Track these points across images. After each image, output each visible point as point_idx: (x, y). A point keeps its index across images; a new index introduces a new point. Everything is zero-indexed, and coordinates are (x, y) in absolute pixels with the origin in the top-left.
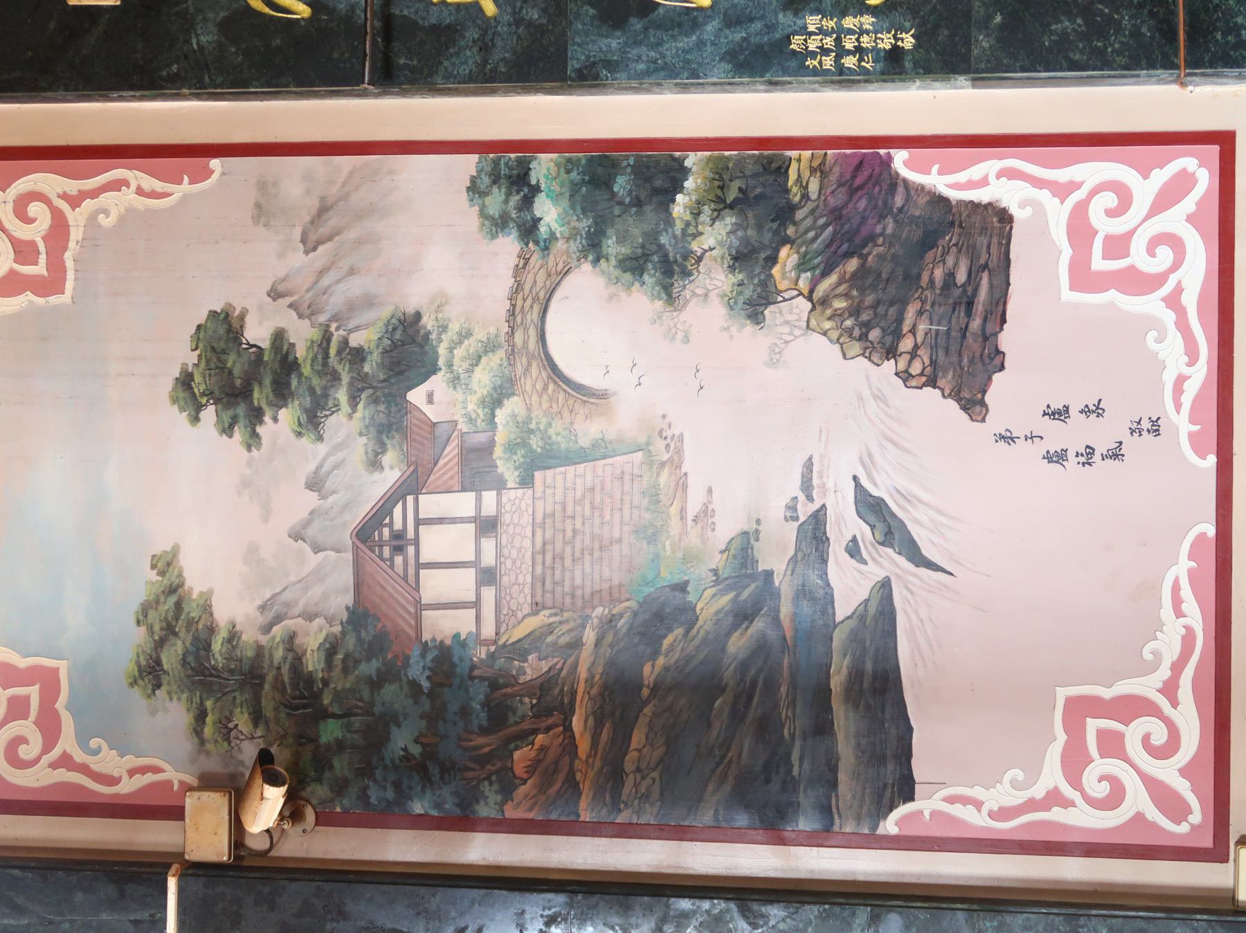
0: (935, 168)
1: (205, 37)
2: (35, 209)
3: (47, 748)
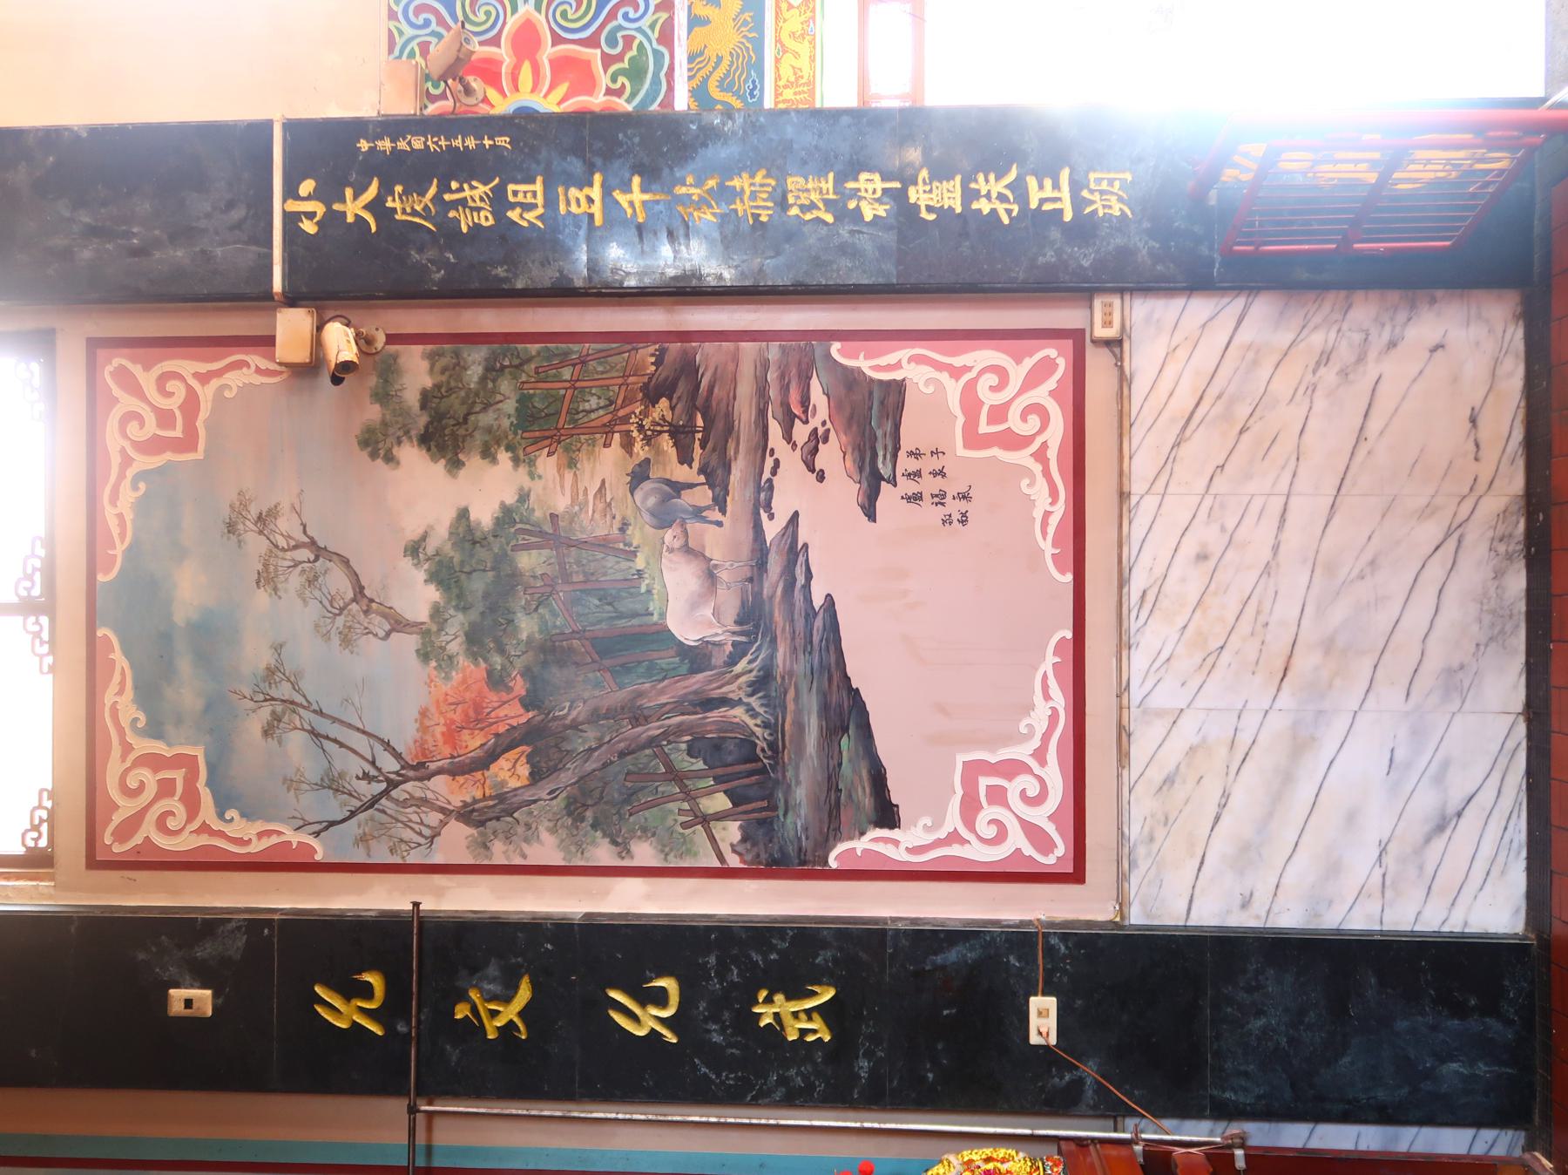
2: (172, 385)
3: (190, 819)
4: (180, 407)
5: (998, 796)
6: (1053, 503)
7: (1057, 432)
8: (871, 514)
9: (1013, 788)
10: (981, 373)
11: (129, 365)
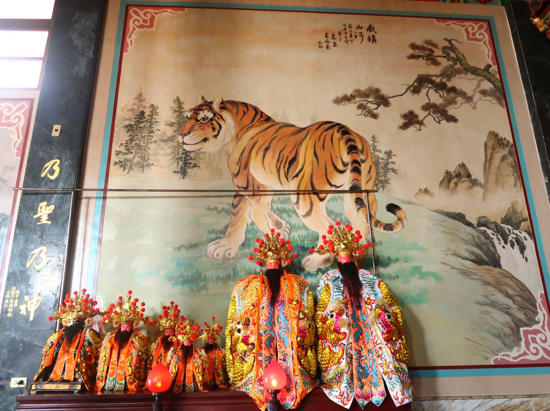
1: (41, 154)
2: (17, 120)
5: (145, 21)
7: (531, 358)
8: (445, 39)
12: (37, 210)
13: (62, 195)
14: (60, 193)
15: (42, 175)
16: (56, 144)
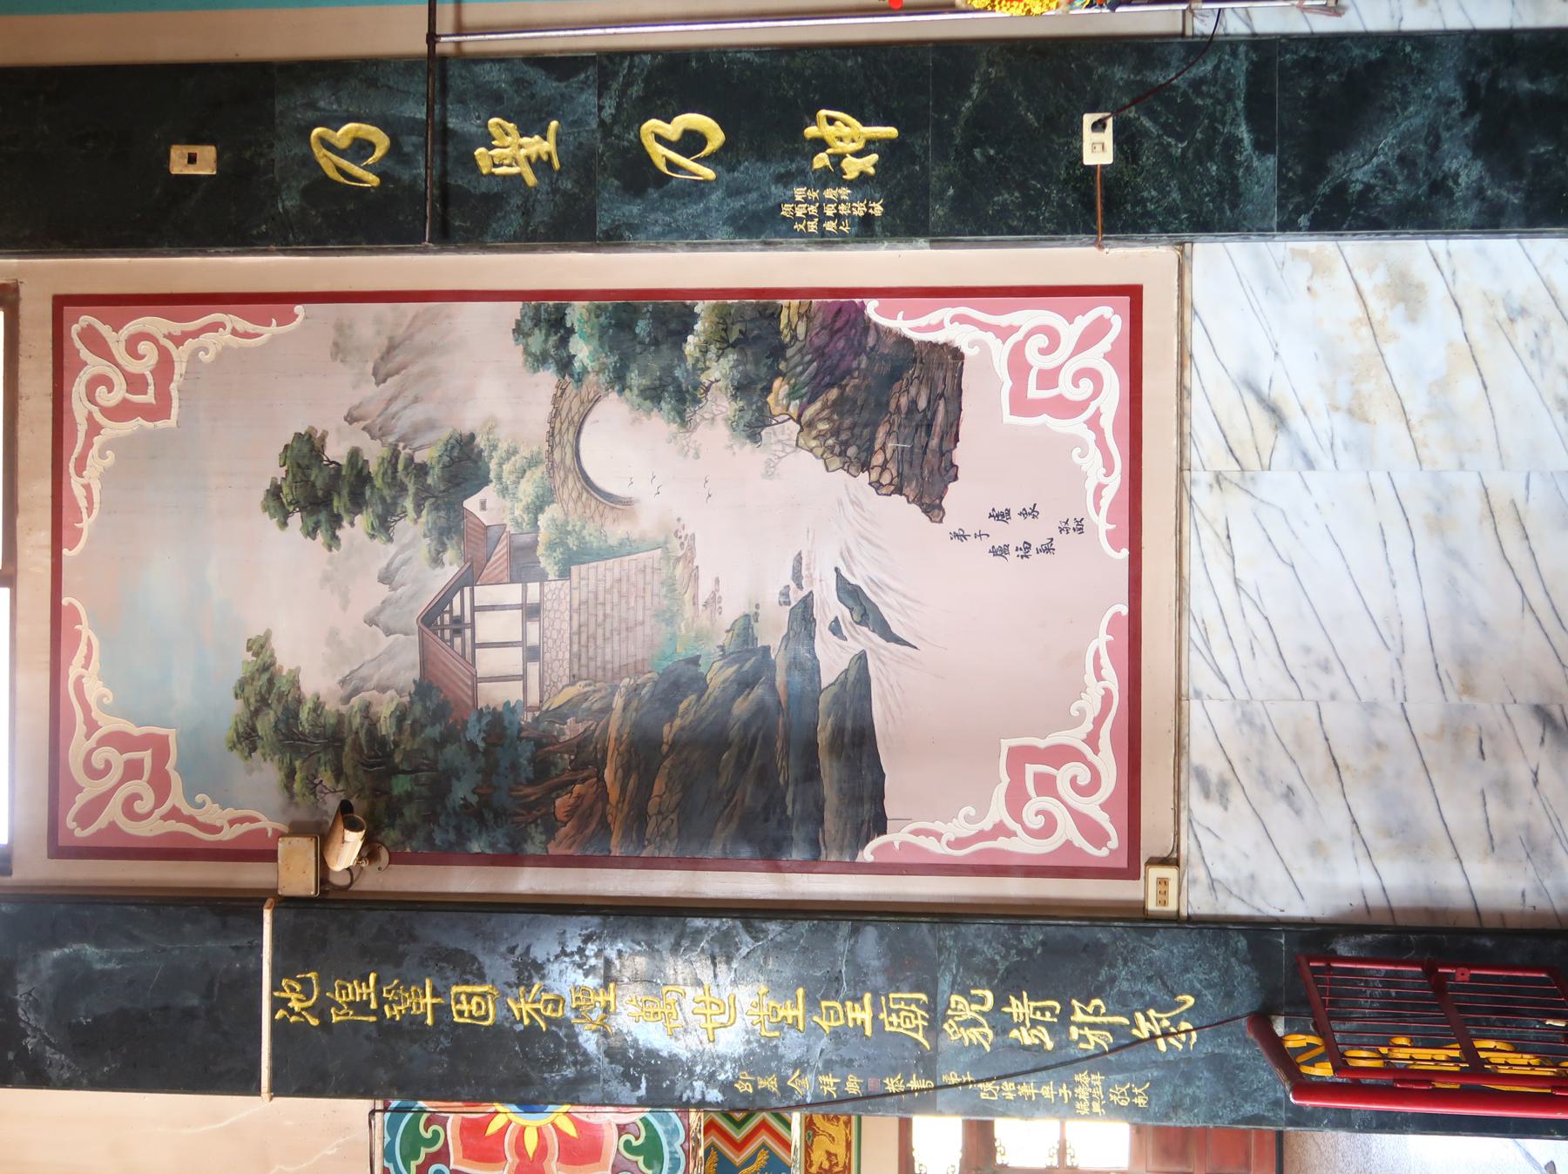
0: (900, 315)
2: (144, 347)
4: (1029, 798)
6: (81, 677)
9: (1063, 775)
10: (150, 814)
11: (98, 325)
12: (504, 177)
13: (451, 96)
14: (444, 106)
15: (372, 180)
16: (248, 154)
